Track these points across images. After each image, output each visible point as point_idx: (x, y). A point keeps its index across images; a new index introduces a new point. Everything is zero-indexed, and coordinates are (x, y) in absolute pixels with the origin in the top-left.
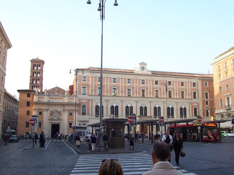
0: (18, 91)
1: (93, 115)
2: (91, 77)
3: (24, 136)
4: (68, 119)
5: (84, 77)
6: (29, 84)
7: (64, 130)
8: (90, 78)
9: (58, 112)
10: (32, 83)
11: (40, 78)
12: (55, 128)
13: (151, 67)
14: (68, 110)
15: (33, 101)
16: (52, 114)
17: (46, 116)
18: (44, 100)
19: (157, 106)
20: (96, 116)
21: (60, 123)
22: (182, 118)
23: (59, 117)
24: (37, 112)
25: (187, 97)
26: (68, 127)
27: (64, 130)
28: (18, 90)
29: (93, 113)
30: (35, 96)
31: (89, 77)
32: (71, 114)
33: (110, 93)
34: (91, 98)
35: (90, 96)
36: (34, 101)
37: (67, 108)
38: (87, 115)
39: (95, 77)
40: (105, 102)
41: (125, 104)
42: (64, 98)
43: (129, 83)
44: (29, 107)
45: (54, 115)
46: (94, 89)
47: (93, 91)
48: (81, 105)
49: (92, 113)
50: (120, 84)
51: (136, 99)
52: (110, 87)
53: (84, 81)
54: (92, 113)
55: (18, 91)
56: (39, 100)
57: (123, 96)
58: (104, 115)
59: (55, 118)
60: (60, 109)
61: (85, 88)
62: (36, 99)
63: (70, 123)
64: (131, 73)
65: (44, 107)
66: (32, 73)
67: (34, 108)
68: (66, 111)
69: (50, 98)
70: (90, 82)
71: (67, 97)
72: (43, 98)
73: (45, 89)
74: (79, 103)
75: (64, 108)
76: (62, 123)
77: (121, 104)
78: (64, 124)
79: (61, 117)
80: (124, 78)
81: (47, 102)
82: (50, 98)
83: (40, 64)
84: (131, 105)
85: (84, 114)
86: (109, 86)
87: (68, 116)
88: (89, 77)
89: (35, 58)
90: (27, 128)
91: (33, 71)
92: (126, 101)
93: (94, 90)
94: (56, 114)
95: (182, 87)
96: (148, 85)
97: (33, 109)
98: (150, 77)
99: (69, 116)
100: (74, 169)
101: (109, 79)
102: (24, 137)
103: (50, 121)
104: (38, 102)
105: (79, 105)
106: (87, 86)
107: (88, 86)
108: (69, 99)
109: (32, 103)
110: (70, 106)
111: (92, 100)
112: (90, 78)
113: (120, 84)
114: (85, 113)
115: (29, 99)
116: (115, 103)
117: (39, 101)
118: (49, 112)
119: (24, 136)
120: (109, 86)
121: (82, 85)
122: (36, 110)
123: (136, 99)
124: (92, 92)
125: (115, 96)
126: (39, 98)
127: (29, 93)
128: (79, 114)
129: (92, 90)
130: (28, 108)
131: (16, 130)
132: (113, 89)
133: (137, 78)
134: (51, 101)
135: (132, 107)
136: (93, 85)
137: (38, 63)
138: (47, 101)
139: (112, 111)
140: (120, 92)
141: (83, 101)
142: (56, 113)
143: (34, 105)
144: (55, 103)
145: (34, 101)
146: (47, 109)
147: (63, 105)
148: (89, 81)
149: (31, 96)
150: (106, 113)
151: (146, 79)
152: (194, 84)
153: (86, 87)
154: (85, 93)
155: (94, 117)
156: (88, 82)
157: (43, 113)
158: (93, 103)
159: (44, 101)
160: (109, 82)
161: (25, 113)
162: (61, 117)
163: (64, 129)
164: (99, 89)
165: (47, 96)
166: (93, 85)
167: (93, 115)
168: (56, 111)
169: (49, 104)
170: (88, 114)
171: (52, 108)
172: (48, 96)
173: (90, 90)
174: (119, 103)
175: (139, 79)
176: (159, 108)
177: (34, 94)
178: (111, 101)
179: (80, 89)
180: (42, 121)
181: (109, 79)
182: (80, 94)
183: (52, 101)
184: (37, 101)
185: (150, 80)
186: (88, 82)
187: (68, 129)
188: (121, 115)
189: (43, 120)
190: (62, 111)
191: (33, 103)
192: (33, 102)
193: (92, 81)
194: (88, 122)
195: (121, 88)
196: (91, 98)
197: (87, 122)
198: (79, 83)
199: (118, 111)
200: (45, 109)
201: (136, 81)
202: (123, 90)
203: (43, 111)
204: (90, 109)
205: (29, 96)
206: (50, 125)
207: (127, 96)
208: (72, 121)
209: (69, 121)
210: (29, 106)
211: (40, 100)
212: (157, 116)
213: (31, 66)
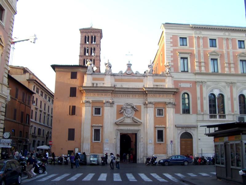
0: (54, 67)
1: (206, 114)
2: (195, 37)
3: (64, 158)
4: (93, 121)
6: (79, 57)
7: (147, 147)
8: (195, 41)
9: (133, 107)
10: (83, 54)
12: (128, 142)
14: (155, 104)
15: (82, 86)
16: (121, 111)
17: (109, 115)
18: (104, 84)
19: (216, 93)
20: (211, 117)
21: (139, 130)
22: (215, 117)
23: (135, 118)
24: (90, 108)
26: (155, 140)
27: (147, 145)
28: (52, 64)
30: (86, 77)
31: (191, 38)
32: (98, 111)
33: (236, 68)
34: (199, 78)
35: (196, 74)
36: (84, 85)
37: (151, 99)
38: (194, 113)
40: (227, 87)
41: (207, 88)
42: (144, 80)
43: (240, 48)
44: (74, 98)
45: (126, 115)
46: (202, 60)
47: (203, 64)
48: (180, 93)
50: (195, 49)
52: (235, 57)
53: (183, 45)
55: (54, 67)
56: (93, 84)
57: (232, 73)
58: (226, 112)
59: (128, 121)
60: (136, 101)
61: (185, 61)
62: (88, 81)
63: (158, 131)
65: (105, 98)
67: (84, 99)
68: (151, 105)
69: (116, 80)
70: (200, 49)
71: (151, 77)
73: (107, 62)
74: (177, 89)
75: (147, 100)
76: (142, 131)
78: (147, 133)
79: (141, 119)
80: (202, 36)
81: (111, 87)
82: (116, 80)
84: (220, 91)
85: (186, 111)
86: (231, 54)
87: (155, 116)
88: (191, 38)
90: (71, 142)
93: (205, 62)
94: (130, 113)
95: (213, 49)
97: (83, 103)
99: (157, 116)
101: (230, 42)
102: (64, 160)
103: (117, 127)
104: (93, 87)
105: (175, 92)
106: (190, 56)
107: (192, 54)
109: (81, 91)
110: (158, 95)
111: (202, 82)
112: (195, 41)
113: (195, 49)
115: (75, 83)
117: (95, 85)
118: (115, 107)
119: (64, 158)
120: (231, 54)
121: (180, 53)
122: (88, 104)
124: (200, 67)
125: (215, 73)
126: (94, 79)
127: (74, 70)
128: (177, 112)
129: (200, 63)
130: (74, 102)
131: (49, 145)
132: (181, 58)
135: (222, 96)
136: (202, 54)
138: (110, 86)
139: (212, 104)
140: (225, 65)
141: (183, 85)
142: (130, 110)
143: (84, 95)
144: (128, 88)
145: (84, 85)
146: (111, 101)
147: (144, 93)
148: (192, 46)
149: (78, 76)
150: (230, 109)
151: (218, 38)
152: (183, 39)
153: (187, 58)
154: (186, 70)
155: (207, 117)
156: (191, 49)
158: (204, 89)
159: (105, 85)
160: (230, 47)
161: (67, 110)
162: (141, 119)
163: (147, 143)
164: (182, 60)
165: (110, 76)
166: (202, 54)
167: (206, 114)
168: (129, 107)
170: (196, 112)
171: (122, 101)
173: (196, 64)
174: (225, 87)
175: (203, 38)
177: (85, 73)
178: (238, 84)
179: (175, 61)
180: (165, 127)
181: (230, 42)
182: (176, 71)
183: (97, 84)
184: (91, 85)
186: (191, 49)
187: (155, 144)
188: (231, 113)
189: (103, 124)
190: (143, 107)
191: (83, 90)
192: (82, 89)
193: (199, 46)
194: (196, 129)
195: (226, 56)
196: (199, 78)
197: (193, 129)
198: (173, 49)
200: (108, 102)
201: (198, 43)
203: (103, 107)
204: (199, 102)
205: (74, 76)
206: (117, 136)
208: (164, 126)
209: (93, 125)
210: (75, 96)
211: (97, 84)
212: (216, 113)
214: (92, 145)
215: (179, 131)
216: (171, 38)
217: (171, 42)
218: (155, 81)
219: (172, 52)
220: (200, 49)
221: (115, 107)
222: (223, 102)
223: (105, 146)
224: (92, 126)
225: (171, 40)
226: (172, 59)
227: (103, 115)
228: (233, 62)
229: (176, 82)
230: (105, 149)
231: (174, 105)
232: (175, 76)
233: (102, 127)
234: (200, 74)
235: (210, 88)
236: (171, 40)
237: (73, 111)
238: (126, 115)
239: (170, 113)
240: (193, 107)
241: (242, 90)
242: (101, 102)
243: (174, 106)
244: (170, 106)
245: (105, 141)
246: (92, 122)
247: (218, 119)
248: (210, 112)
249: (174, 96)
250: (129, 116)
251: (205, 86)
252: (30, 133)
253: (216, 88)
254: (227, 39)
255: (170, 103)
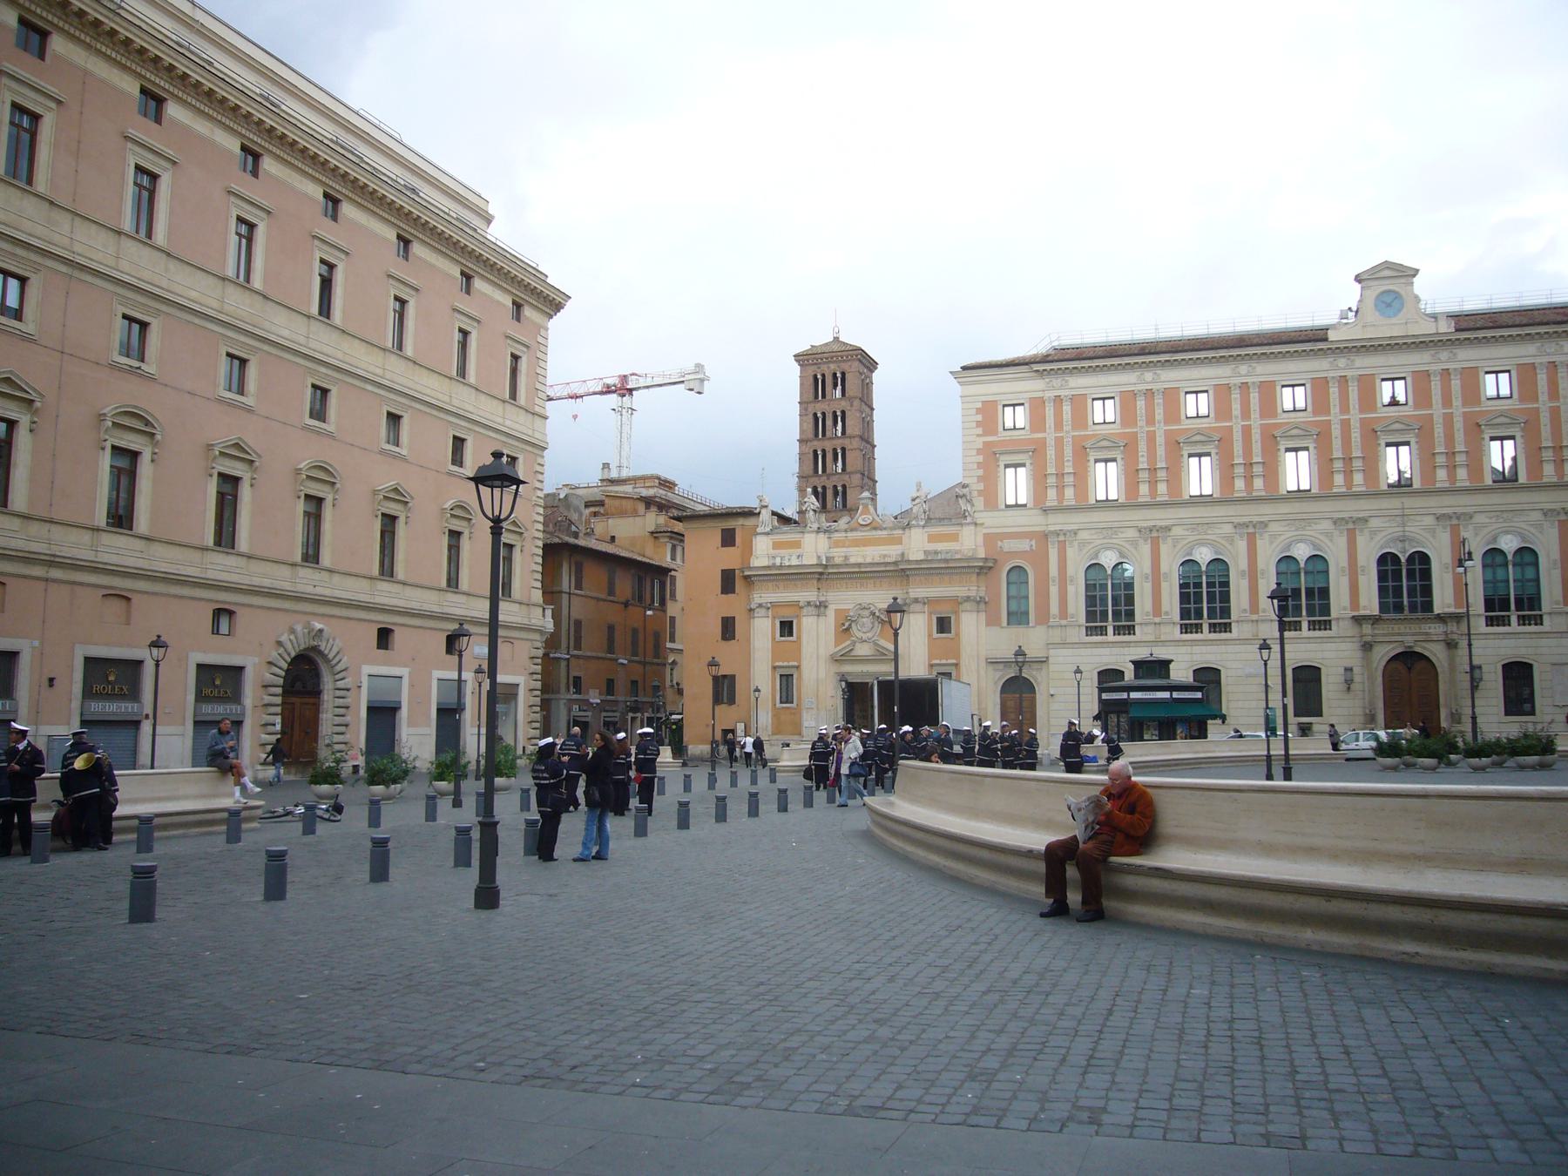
5: (1014, 405)
11: (846, 443)
13: (1451, 283)
14: (774, 605)
16: (845, 628)
17: (817, 636)
19: (1302, 552)
25: (1332, 485)
29: (1165, 607)
32: (787, 628)
37: (919, 591)
38: (1038, 623)
39: (1073, 398)
40: (1141, 541)
47: (1258, 469)
49: (1063, 613)
51: (1349, 508)
54: (1063, 613)
58: (1138, 617)
59: (863, 650)
64: (1310, 340)
66: (810, 418)
68: (917, 607)
72: (797, 545)
77: (1242, 545)
80: (1256, 379)
83: (845, 367)
85: (1018, 617)
87: (930, 635)
89: (822, 338)
91: (811, 409)
92: (1273, 527)
96: (1430, 406)
98: (1444, 355)
100: (225, 815)
103: (835, 668)
105: (985, 569)
108: (932, 539)
114: (1027, 613)
116: (1201, 543)
123: (1349, 508)
128: (992, 621)
130: (731, 605)
133: (1349, 373)
134: (838, 554)
137: (832, 366)
141: (1009, 545)
142: (867, 621)
144: (859, 565)
155: (1079, 634)
157: (958, 620)
161: (398, 637)
168: (866, 613)
169: (823, 574)
170: (1044, 618)
171: (845, 599)
172: (821, 535)
174: (1230, 539)
176: (1528, 558)
183: (846, 558)
185: (1058, 400)
189: (799, 660)
196: (1056, 522)
199: (1380, 597)
202: (1049, 471)
203: (956, 613)
204: (1054, 590)
207: (1490, 482)
212: (1508, 609)
213: (802, 385)
214: (776, 714)
215: (998, 674)
216: (978, 411)
217: (979, 424)
218: (932, 539)
219: (979, 452)
220: (1539, 405)
221: (831, 613)
222: (1426, 574)
223: (805, 715)
224: (774, 668)
225: (979, 418)
226: (980, 472)
227: (958, 635)
228: (1260, 460)
229: (990, 539)
230: (806, 724)
231: (980, 601)
232: (988, 522)
233: (798, 667)
234: (1061, 509)
235: (1486, 531)
236: (979, 418)
237: (728, 628)
238: (859, 635)
239: (970, 625)
240: (1036, 607)
241: (1290, 545)
242: (796, 605)
243: (982, 606)
244: (967, 606)
245: (806, 702)
246: (774, 658)
247: (1111, 637)
248: (1184, 614)
249: (982, 577)
250: (865, 637)
251: (1266, 536)
252: (668, 683)
253: (1507, 532)
254: (1149, 393)
255: (968, 599)
